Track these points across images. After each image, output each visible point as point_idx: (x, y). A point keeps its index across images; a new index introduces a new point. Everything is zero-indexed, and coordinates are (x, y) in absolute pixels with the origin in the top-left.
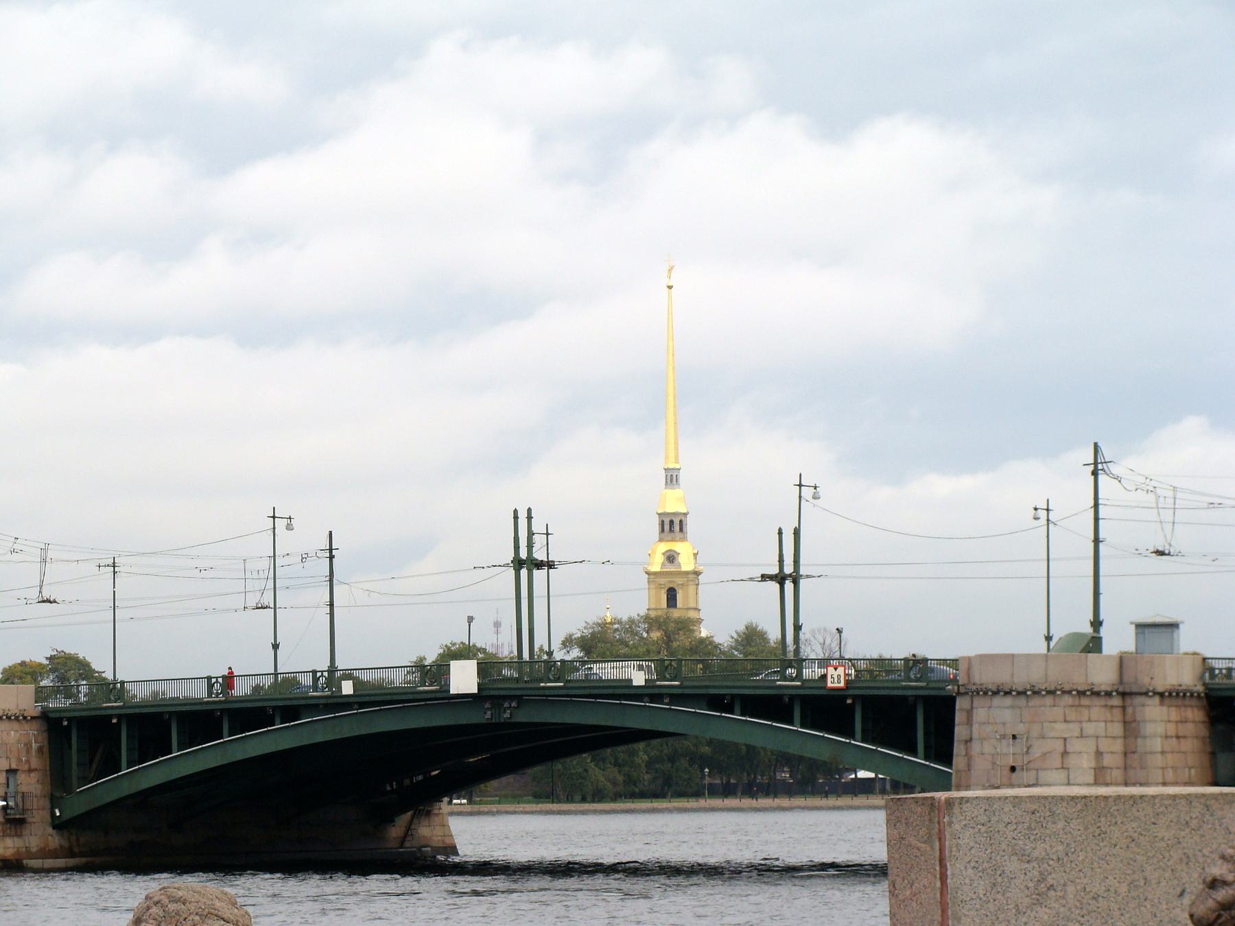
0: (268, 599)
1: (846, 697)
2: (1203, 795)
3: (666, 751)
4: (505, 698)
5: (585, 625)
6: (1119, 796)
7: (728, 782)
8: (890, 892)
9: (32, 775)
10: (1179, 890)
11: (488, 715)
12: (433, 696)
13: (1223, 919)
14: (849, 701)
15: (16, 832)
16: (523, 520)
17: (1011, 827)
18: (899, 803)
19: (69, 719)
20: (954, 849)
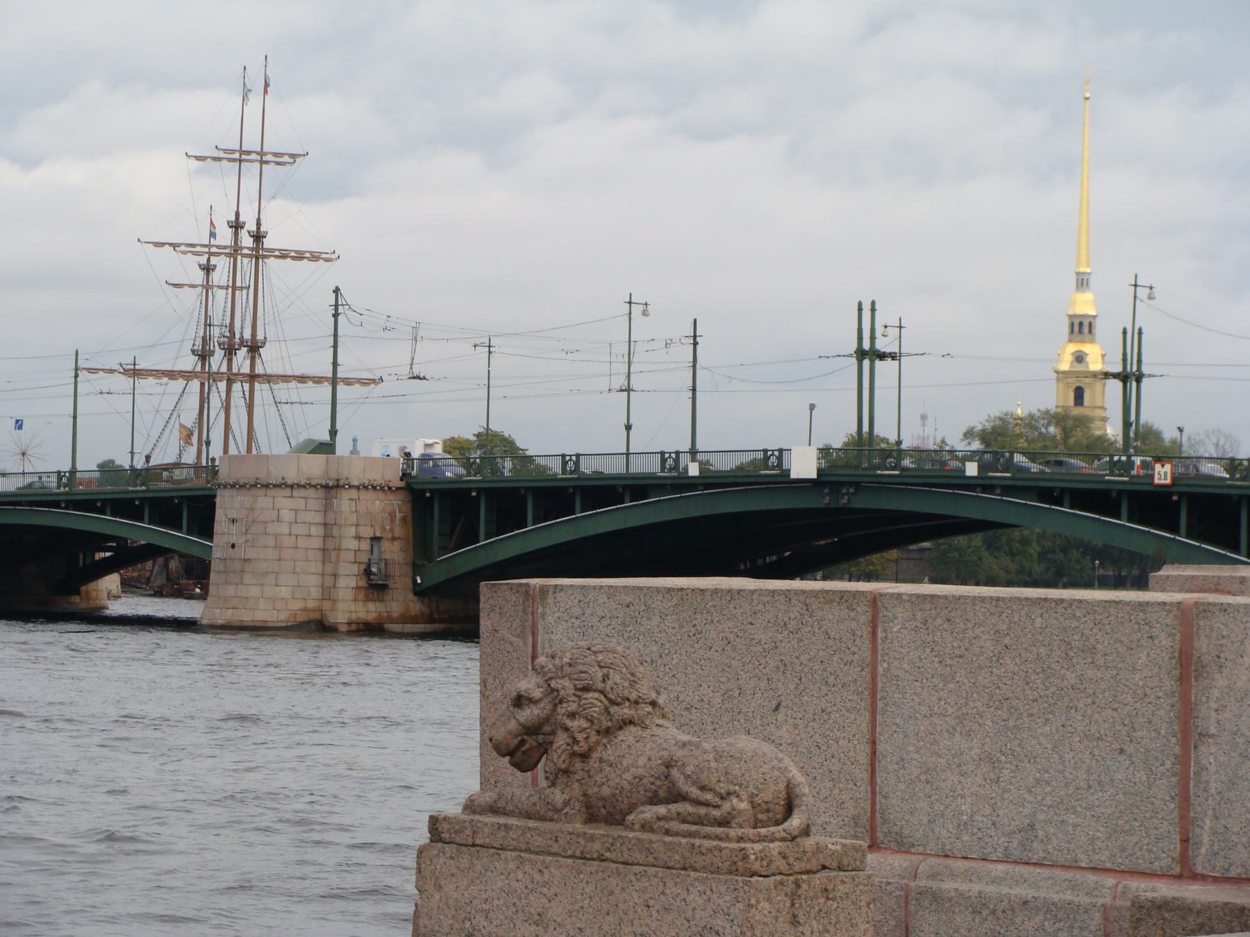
1: (1172, 494)
2: (803, 592)
3: (1058, 542)
4: (843, 484)
5: (987, 417)
6: (716, 589)
7: (1119, 574)
8: (481, 692)
9: (395, 543)
10: (774, 703)
11: (827, 500)
12: (774, 479)
13: (527, 746)
14: (1175, 498)
15: (378, 596)
16: (866, 311)
17: (604, 622)
18: (493, 590)
19: (431, 491)
20: (547, 646)
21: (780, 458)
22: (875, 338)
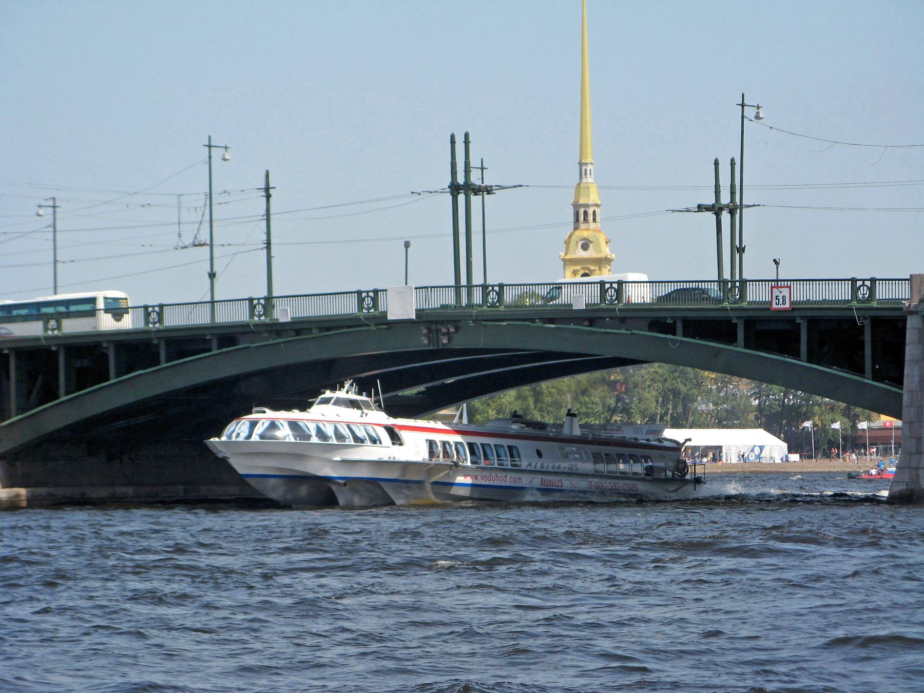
0: (204, 237)
21: (375, 300)
22: (456, 173)
